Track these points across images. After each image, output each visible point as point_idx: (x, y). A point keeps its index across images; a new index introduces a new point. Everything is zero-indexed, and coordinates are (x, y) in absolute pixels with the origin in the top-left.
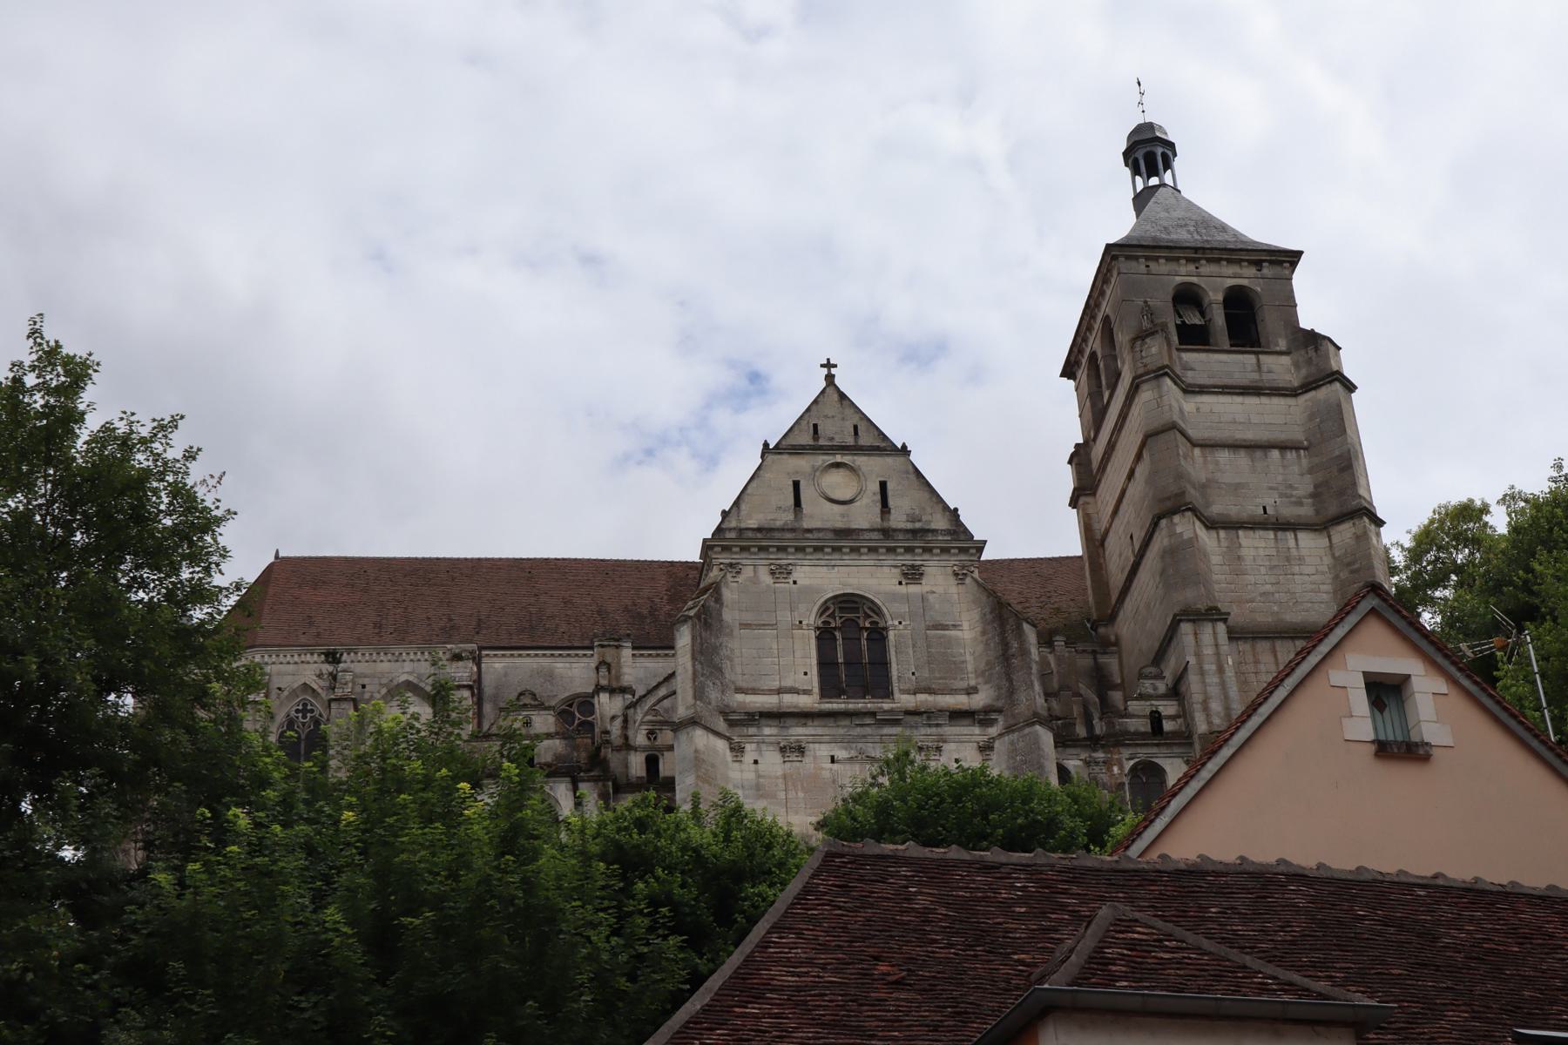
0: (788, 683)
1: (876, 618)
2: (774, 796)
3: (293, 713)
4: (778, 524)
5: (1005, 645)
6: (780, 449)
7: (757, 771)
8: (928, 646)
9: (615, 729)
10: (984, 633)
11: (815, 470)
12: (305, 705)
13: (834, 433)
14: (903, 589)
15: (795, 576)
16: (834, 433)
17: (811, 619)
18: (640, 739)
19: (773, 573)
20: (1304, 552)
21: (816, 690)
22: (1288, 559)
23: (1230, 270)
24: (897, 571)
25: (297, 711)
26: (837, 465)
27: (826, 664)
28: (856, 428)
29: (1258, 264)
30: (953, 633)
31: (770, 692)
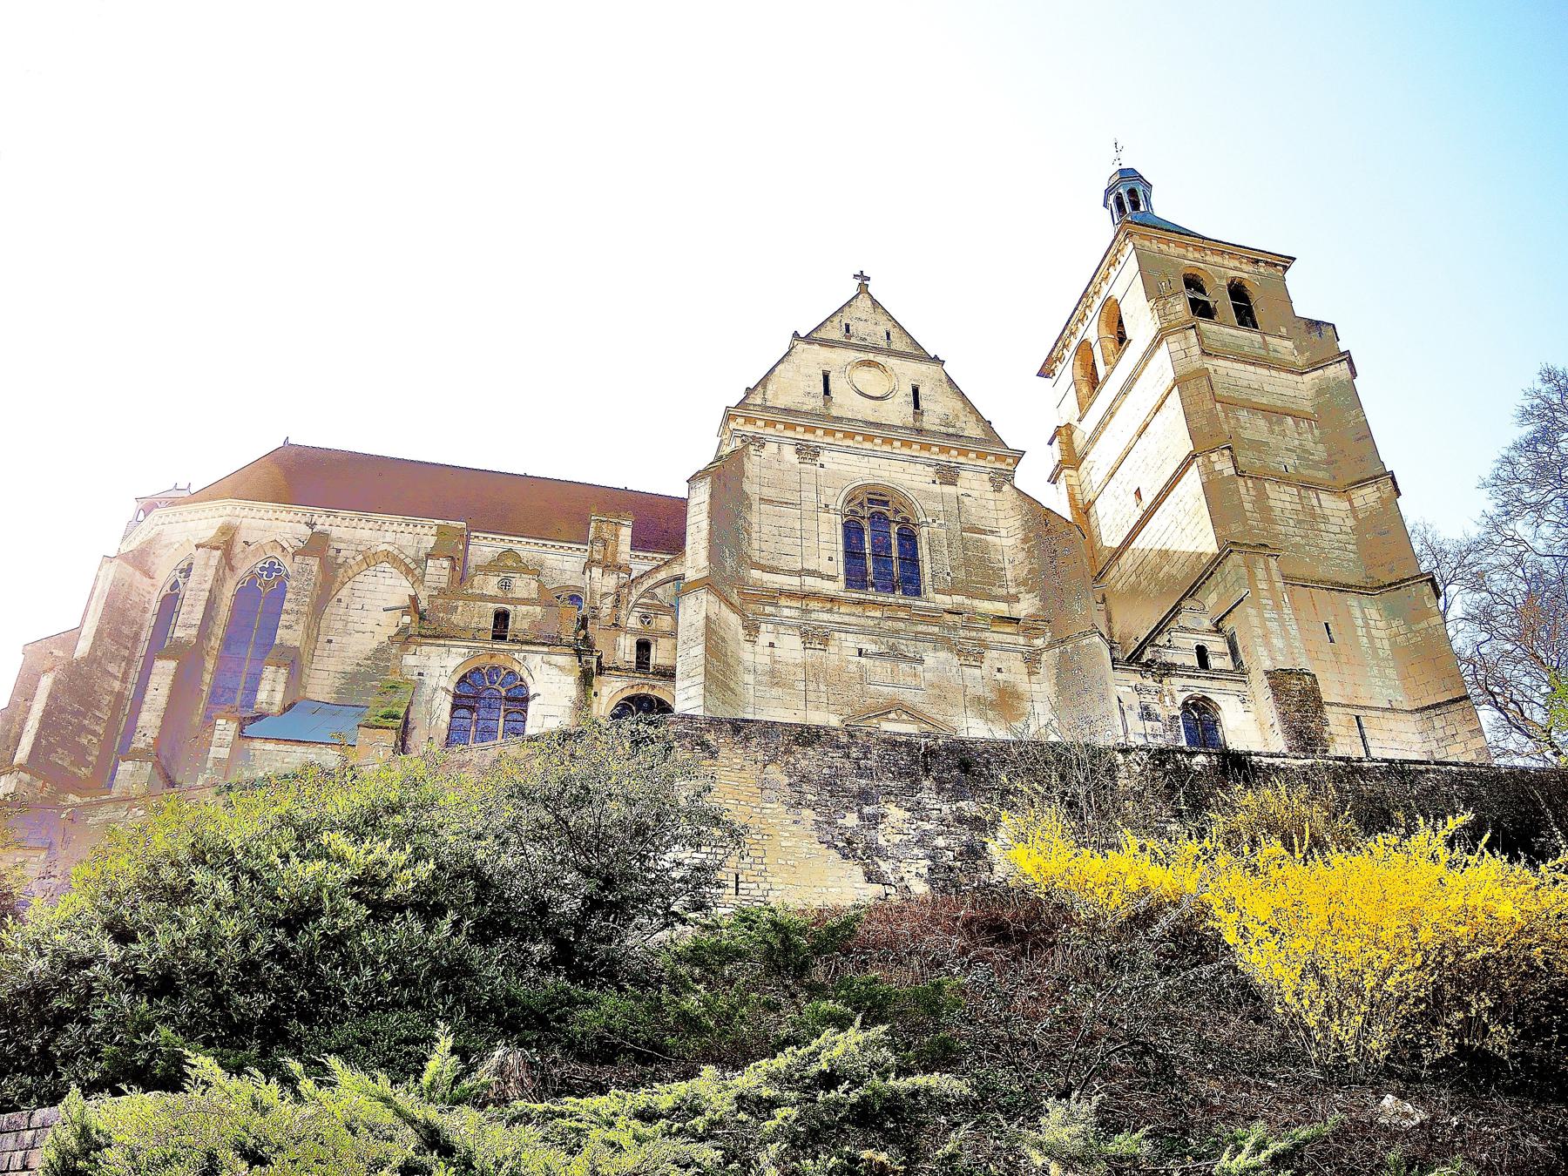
0: (811, 565)
2: (792, 687)
4: (805, 408)
6: (809, 339)
7: (771, 655)
8: (965, 548)
9: (606, 607)
10: (1025, 541)
13: (862, 330)
14: (937, 488)
16: (862, 330)
19: (798, 451)
20: (1327, 512)
21: (842, 577)
22: (1313, 515)
27: (853, 554)
30: (990, 538)
31: (791, 573)
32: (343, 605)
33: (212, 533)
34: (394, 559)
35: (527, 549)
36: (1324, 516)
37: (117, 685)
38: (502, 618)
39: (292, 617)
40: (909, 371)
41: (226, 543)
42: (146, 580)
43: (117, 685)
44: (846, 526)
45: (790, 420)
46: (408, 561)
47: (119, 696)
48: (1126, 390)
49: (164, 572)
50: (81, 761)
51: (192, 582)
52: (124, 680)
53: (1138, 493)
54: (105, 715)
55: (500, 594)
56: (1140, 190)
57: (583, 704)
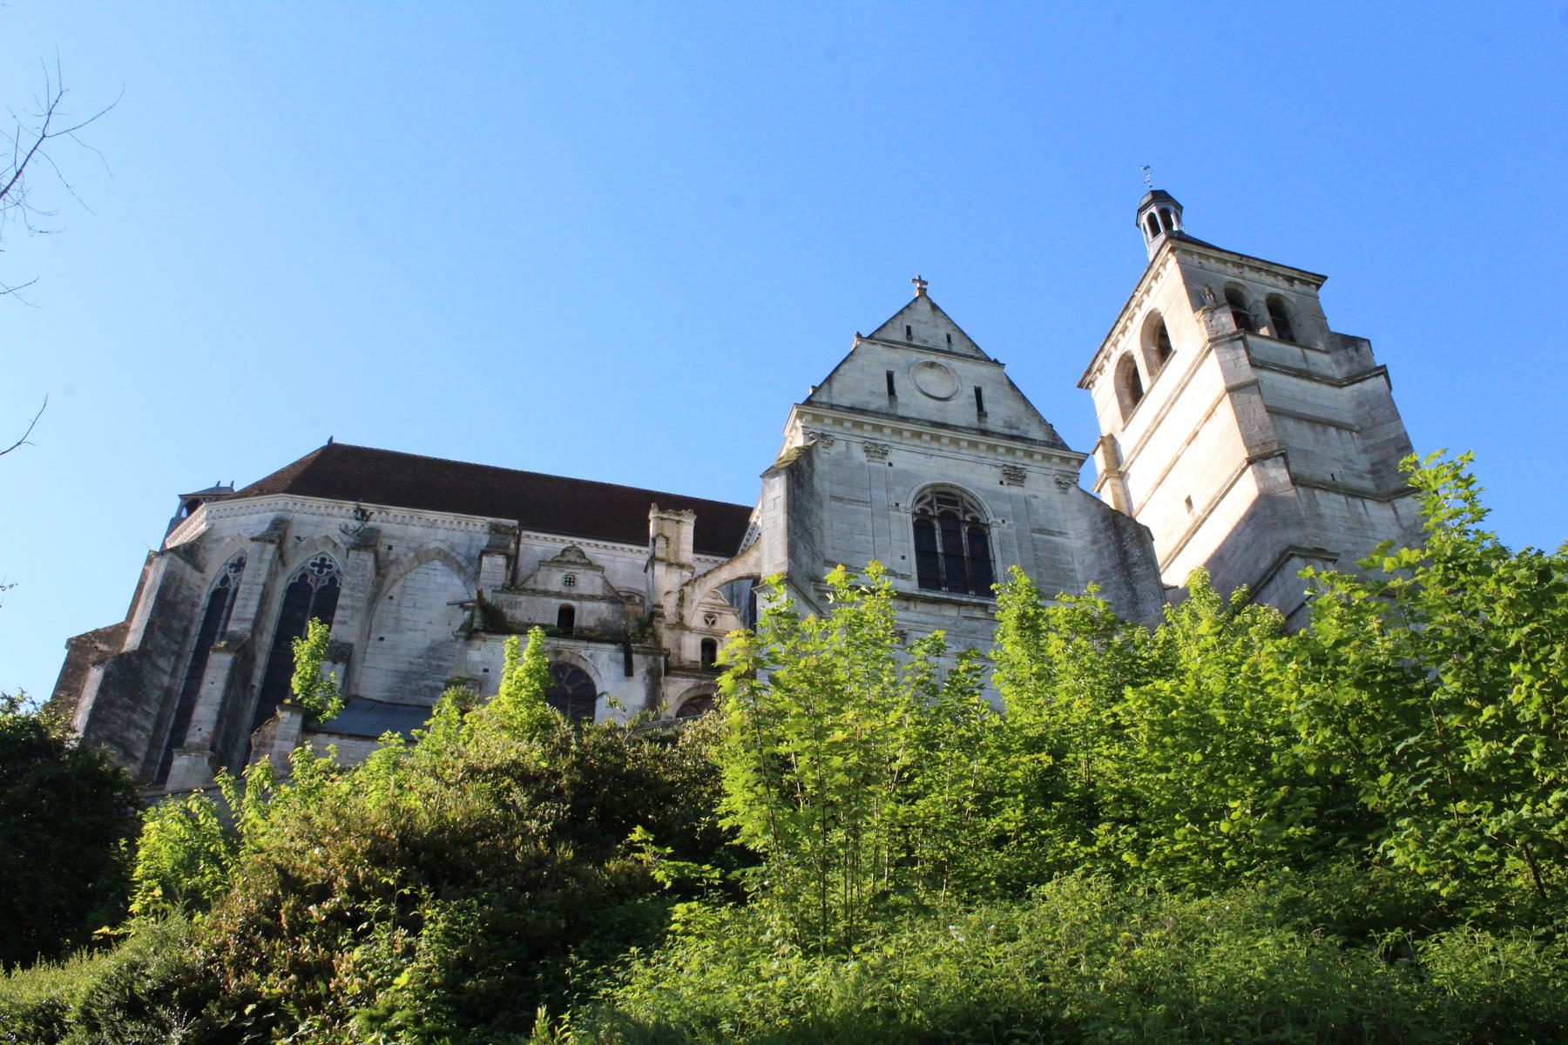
1: (976, 514)
3: (309, 566)
4: (872, 407)
5: (1123, 554)
8: (1035, 550)
10: (1095, 541)
11: (910, 366)
12: (323, 560)
14: (1005, 489)
15: (889, 458)
17: (908, 503)
18: (696, 619)
19: (867, 450)
21: (915, 576)
22: (1361, 523)
23: (1270, 280)
24: (998, 471)
25: (314, 565)
26: (932, 365)
28: (949, 337)
29: (1291, 280)
30: (1058, 539)
32: (395, 602)
33: (266, 527)
34: (445, 557)
35: (593, 549)
36: (1372, 525)
37: (166, 680)
38: (567, 614)
39: (348, 612)
40: (972, 373)
41: (278, 532)
42: (196, 574)
43: (166, 680)
44: (915, 525)
45: (860, 418)
46: (460, 559)
47: (168, 692)
48: (1173, 401)
49: (216, 565)
50: (128, 755)
51: (246, 574)
52: (173, 674)
53: (1189, 501)
54: (154, 710)
55: (565, 590)
56: (1172, 209)
57: (653, 700)
